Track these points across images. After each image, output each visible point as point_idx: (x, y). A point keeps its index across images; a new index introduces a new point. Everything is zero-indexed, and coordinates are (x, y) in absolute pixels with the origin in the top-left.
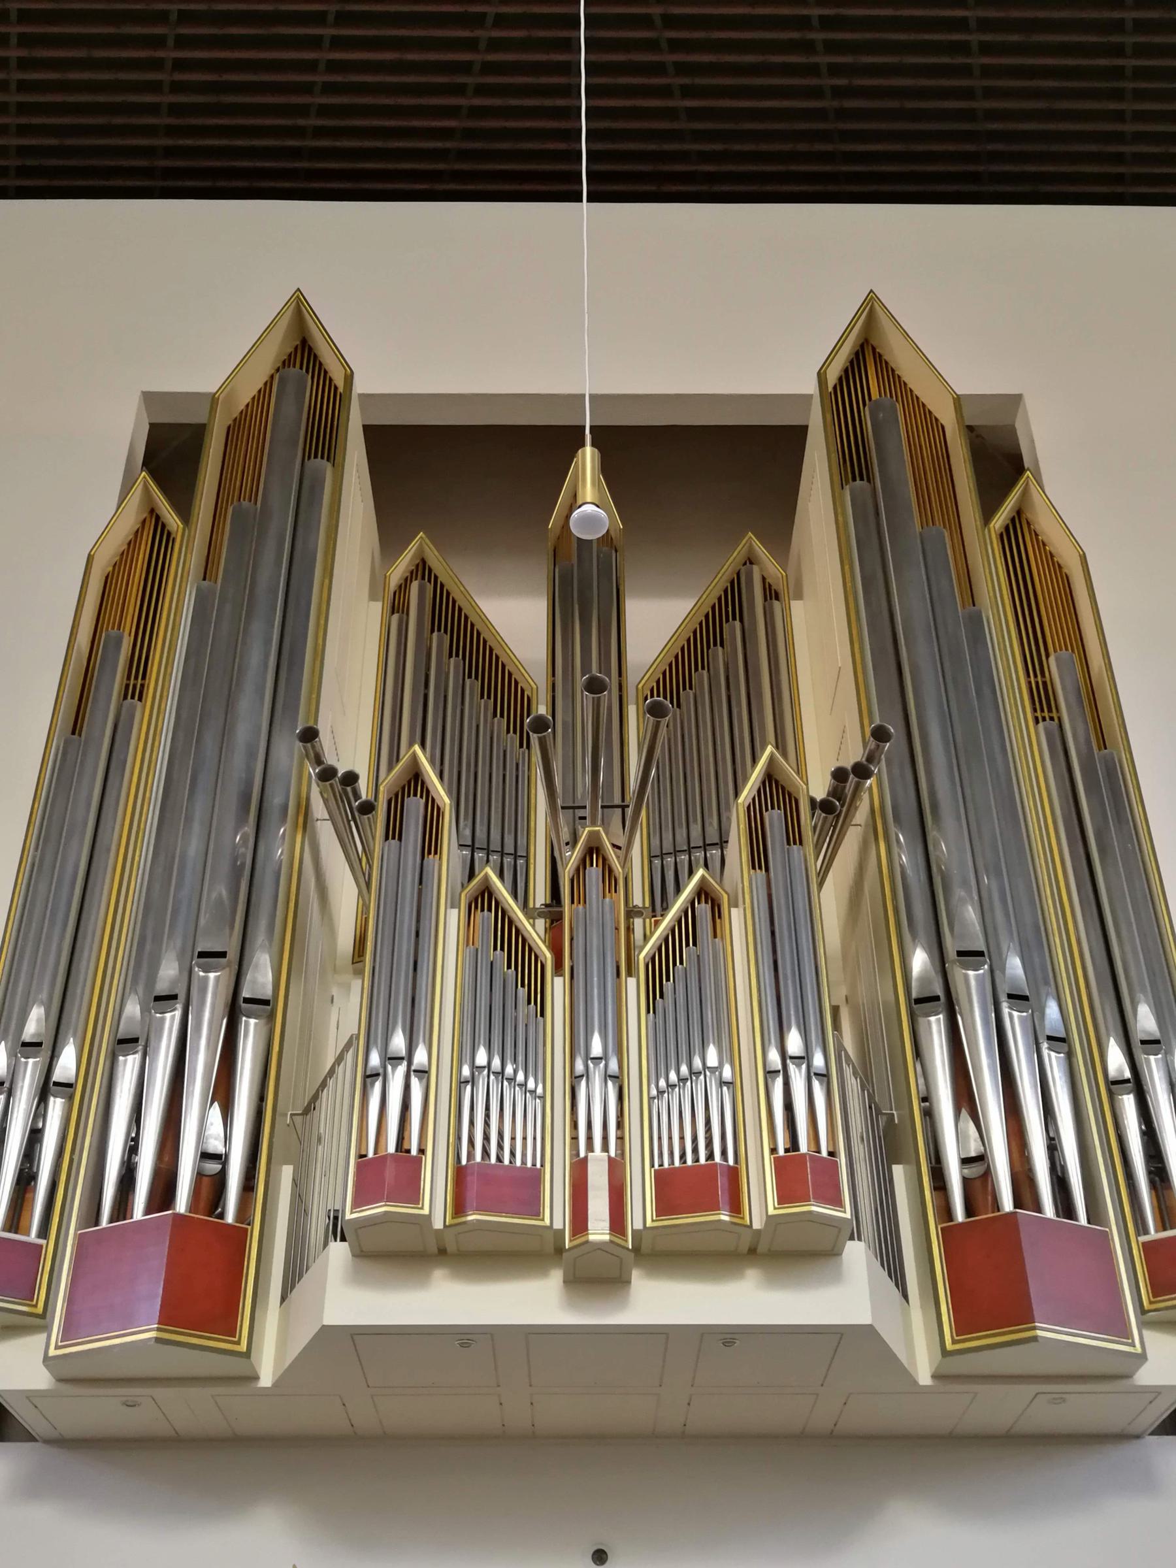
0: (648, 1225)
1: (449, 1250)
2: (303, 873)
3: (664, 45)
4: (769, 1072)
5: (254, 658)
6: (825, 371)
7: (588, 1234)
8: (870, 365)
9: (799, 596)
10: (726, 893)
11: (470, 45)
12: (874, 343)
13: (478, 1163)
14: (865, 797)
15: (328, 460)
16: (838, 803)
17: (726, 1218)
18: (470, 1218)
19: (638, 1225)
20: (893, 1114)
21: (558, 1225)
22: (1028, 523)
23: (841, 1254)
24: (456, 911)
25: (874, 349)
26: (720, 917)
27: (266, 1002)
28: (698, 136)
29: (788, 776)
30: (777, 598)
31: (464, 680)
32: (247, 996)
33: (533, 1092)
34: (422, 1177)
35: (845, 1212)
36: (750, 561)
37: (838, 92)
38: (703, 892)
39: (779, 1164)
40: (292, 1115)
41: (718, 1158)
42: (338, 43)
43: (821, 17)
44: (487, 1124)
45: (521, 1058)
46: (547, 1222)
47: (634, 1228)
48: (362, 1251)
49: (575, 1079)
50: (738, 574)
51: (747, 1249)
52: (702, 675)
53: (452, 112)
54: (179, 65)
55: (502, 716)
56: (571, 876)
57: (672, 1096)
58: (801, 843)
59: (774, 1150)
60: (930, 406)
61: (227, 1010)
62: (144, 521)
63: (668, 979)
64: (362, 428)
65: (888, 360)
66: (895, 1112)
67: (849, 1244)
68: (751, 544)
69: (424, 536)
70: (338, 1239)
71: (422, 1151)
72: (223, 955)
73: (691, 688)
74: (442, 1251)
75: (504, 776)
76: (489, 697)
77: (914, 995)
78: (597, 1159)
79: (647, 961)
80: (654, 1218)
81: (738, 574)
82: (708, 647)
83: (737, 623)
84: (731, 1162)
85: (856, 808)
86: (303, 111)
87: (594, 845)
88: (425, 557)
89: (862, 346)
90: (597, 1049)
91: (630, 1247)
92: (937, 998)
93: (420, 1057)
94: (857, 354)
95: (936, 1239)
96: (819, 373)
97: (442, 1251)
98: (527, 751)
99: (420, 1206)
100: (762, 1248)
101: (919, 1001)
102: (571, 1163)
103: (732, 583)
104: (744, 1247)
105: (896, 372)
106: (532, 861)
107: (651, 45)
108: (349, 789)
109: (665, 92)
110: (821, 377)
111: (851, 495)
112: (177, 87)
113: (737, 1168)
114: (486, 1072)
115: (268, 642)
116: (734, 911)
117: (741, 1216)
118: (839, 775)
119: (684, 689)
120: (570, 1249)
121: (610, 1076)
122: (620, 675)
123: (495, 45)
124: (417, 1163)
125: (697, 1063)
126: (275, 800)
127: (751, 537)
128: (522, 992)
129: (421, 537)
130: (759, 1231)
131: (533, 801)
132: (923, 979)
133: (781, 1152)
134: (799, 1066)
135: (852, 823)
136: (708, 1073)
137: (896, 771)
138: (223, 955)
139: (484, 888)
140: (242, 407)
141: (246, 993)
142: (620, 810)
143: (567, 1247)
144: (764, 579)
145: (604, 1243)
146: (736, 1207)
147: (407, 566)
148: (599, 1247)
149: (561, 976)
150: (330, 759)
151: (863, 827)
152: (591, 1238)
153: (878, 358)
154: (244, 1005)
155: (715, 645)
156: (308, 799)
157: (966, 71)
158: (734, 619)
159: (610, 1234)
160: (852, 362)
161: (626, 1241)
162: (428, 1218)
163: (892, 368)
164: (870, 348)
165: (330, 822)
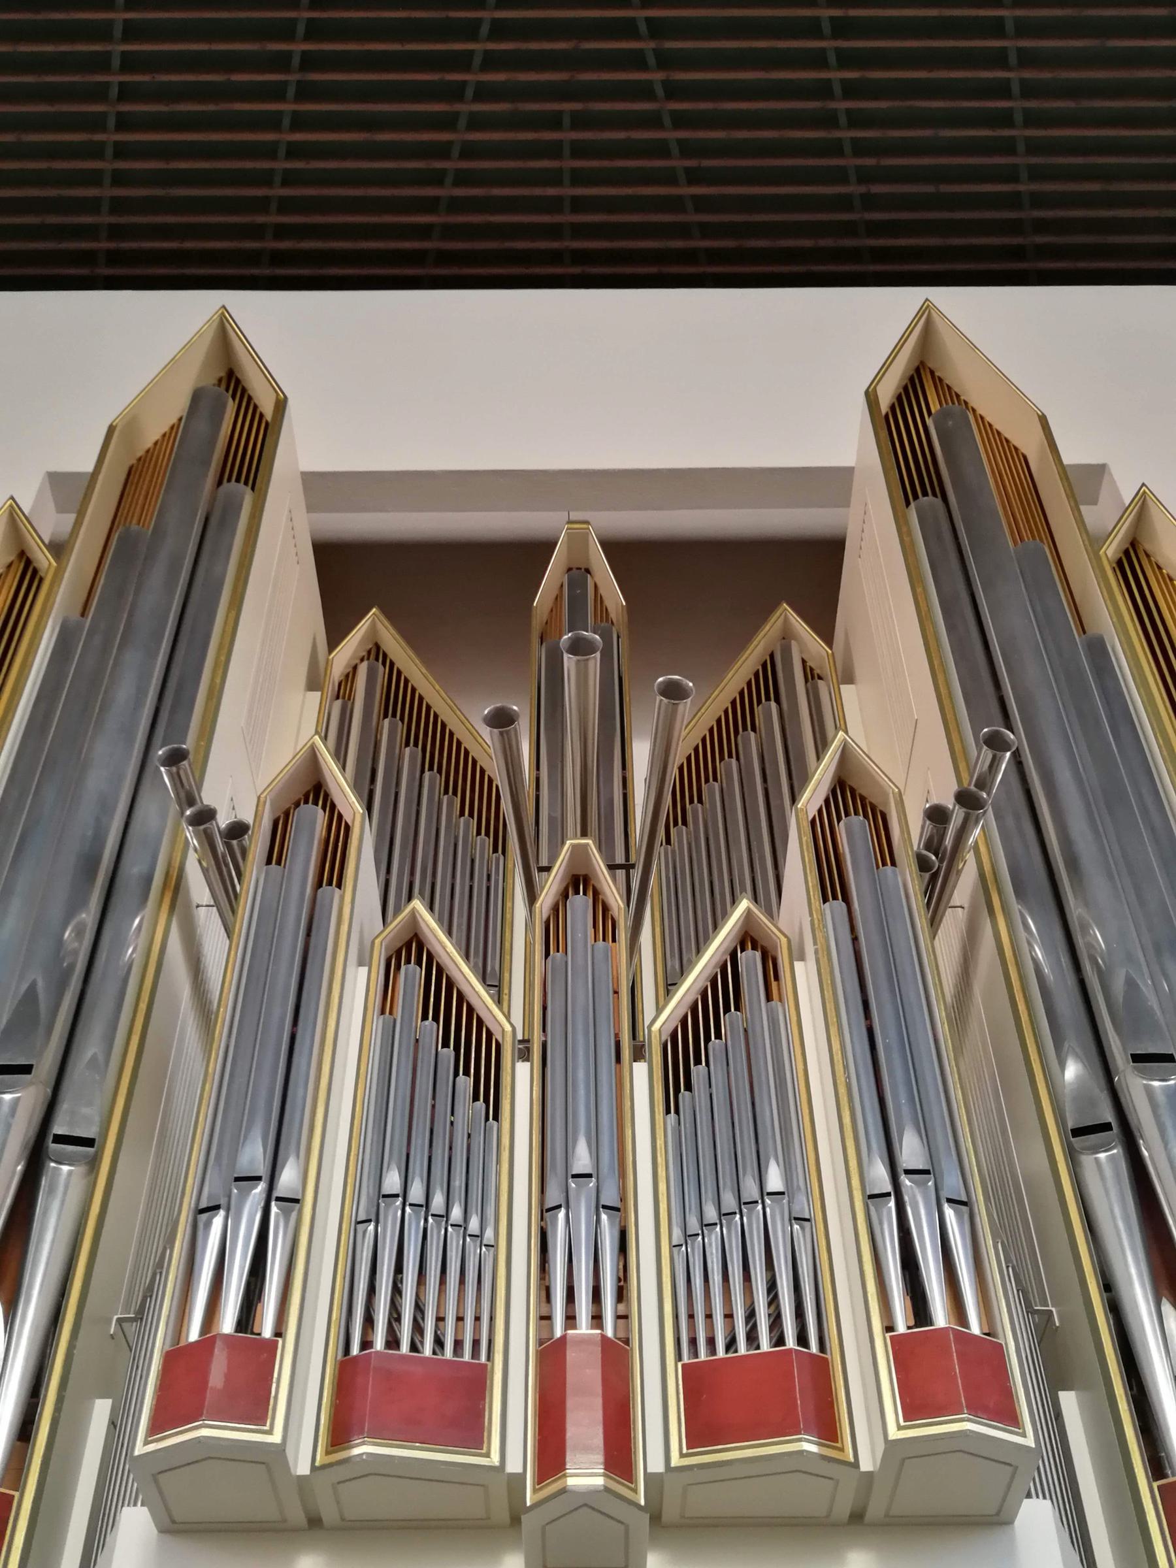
0: (673, 1465)
1: (326, 1519)
2: (164, 968)
3: (667, 121)
4: (871, 1197)
5: (124, 693)
6: (875, 387)
7: (565, 1476)
8: (929, 386)
9: (849, 678)
10: (786, 936)
11: (447, 122)
12: (930, 365)
13: (377, 1352)
14: (970, 857)
15: (246, 483)
16: (934, 858)
17: (813, 1448)
18: (356, 1451)
19: (656, 1465)
20: (1051, 1311)
21: (514, 1466)
22: (1148, 556)
23: (1009, 1522)
24: (364, 970)
25: (932, 373)
26: (777, 978)
27: (89, 1142)
28: (706, 230)
29: (872, 777)
30: (820, 678)
31: (423, 772)
32: (60, 1132)
33: (479, 1237)
34: (276, 1375)
35: (1024, 1435)
36: (787, 636)
37: (865, 177)
38: (748, 938)
39: (902, 1350)
40: (119, 1321)
41: (791, 1342)
42: (300, 122)
43: (843, 81)
44: (397, 1290)
45: (458, 1182)
46: (495, 1459)
47: (649, 1470)
48: (174, 1522)
49: (546, 1211)
50: (772, 656)
51: (848, 1515)
52: (730, 764)
53: (430, 206)
54: (121, 151)
55: (471, 815)
56: (545, 917)
57: (710, 1239)
58: (893, 864)
59: (889, 1328)
60: (1007, 434)
61: (26, 1153)
62: (10, 566)
63: (698, 1062)
64: (300, 481)
65: (864, 793)
66: (1054, 1309)
67: (1026, 1502)
68: (786, 615)
69: (378, 613)
70: (139, 1503)
71: (279, 1333)
72: (26, 1069)
73: (715, 779)
74: (315, 1522)
75: (471, 887)
76: (455, 793)
77: (1071, 1124)
78: (583, 1341)
79: (664, 1039)
80: (685, 1451)
81: (772, 656)
82: (736, 733)
83: (773, 704)
84: (814, 1348)
85: (959, 873)
86: (262, 205)
87: (582, 872)
88: (379, 642)
89: (918, 370)
90: (582, 1160)
91: (642, 1503)
92: (1106, 1127)
93: (288, 1178)
94: (911, 379)
95: (1151, 1506)
96: (867, 393)
97: (315, 1522)
98: (502, 857)
99: (267, 1428)
100: (875, 1510)
101: (1078, 1132)
102: (537, 1351)
103: (764, 665)
104: (843, 1509)
105: (962, 398)
106: (506, 991)
107: (653, 121)
108: (235, 842)
109: (669, 178)
110: (871, 398)
111: (917, 513)
112: (119, 179)
113: (826, 1360)
114: (399, 1201)
115: (144, 677)
116: (798, 965)
117: (839, 1445)
118: (937, 815)
119: (707, 781)
120: (535, 1506)
121: (604, 1207)
122: (624, 767)
123: (477, 123)
124: (269, 1350)
125: (750, 1189)
126: (133, 868)
127: (786, 609)
128: (465, 1083)
129: (374, 614)
130: (870, 1474)
131: (507, 945)
132: (1082, 1098)
133: (901, 1328)
134: (922, 1185)
135: (952, 904)
136: (768, 1201)
137: (1010, 821)
138: (26, 1069)
139: (412, 935)
140: (149, 444)
141: (58, 1129)
142: (624, 871)
143: (528, 1504)
144: (804, 662)
145: (593, 1492)
146: (828, 1430)
147: (356, 651)
148: (587, 1501)
149: (527, 1060)
150: (209, 796)
151: (966, 910)
152: (571, 1482)
153: (938, 382)
154: (53, 1147)
155: (745, 729)
156: (182, 869)
157: (1008, 147)
158: (768, 699)
159: (604, 1475)
160: (905, 388)
161: (635, 1491)
162: (279, 1451)
163: (956, 393)
164: (928, 371)
165: (215, 908)
